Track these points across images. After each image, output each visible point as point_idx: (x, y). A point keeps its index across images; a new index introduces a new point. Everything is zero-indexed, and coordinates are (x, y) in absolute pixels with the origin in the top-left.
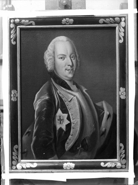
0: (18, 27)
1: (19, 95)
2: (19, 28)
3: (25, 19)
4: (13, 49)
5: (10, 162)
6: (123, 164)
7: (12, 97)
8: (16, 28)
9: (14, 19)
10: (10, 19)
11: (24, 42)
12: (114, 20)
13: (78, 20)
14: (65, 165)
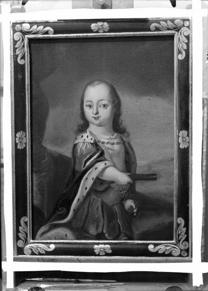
1: (28, 140)
3: (38, 24)
4: (18, 69)
5: (12, 138)
6: (183, 25)
7: (18, 144)
9: (21, 23)
13: (116, 25)
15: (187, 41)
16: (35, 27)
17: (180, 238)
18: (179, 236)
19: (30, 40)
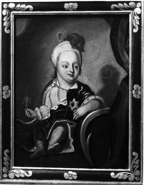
0: (12, 12)
1: (12, 92)
2: (13, 14)
3: (21, 3)
8: (9, 15)
9: (8, 3)
10: (3, 3)
11: (110, 100)
12: (5, 16)
14: (66, 174)
15: (4, 163)
16: (18, 6)
17: (134, 167)
18: (133, 165)
19: (16, 17)
